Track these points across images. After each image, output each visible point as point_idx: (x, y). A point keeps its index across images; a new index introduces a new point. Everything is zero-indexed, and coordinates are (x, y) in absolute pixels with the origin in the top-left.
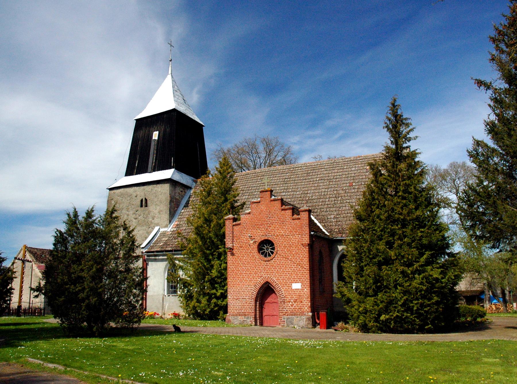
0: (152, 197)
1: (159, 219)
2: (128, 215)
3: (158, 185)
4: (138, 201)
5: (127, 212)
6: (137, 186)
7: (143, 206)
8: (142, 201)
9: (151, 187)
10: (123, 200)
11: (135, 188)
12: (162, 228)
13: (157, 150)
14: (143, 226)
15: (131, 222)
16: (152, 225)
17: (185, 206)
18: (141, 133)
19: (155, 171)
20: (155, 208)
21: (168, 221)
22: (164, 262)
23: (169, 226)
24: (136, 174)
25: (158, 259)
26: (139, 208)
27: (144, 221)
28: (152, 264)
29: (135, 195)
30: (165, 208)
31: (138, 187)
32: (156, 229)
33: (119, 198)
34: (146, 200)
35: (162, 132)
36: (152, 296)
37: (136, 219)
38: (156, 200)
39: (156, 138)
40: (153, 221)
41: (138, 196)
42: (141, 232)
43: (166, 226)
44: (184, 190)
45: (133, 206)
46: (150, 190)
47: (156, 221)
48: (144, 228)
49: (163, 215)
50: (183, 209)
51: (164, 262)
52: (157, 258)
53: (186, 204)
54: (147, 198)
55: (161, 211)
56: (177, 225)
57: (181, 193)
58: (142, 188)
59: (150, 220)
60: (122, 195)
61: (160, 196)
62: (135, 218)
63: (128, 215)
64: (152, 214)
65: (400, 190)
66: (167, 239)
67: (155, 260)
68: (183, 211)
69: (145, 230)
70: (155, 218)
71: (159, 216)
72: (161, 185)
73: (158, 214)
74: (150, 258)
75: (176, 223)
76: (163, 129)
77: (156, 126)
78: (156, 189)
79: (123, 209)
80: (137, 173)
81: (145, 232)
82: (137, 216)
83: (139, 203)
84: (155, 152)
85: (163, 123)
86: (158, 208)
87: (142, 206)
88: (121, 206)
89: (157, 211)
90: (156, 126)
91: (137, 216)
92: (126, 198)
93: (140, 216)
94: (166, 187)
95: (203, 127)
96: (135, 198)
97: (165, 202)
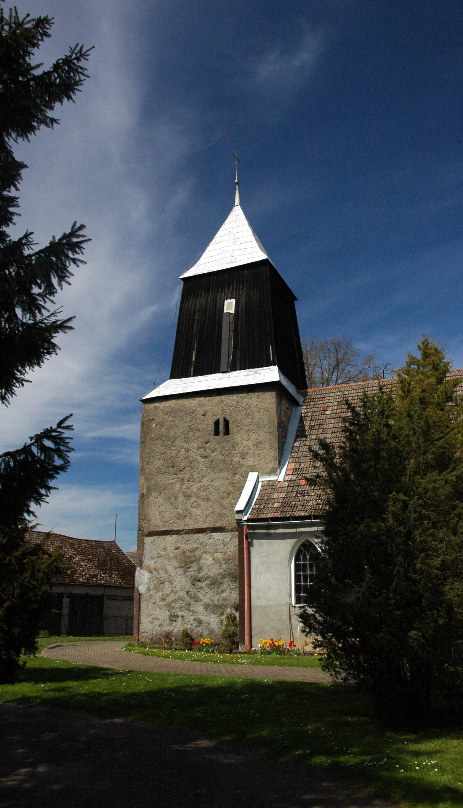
0: (239, 417)
1: (257, 458)
2: (188, 450)
3: (251, 395)
4: (209, 423)
5: (186, 445)
6: (205, 397)
7: (221, 433)
8: (217, 423)
9: (234, 398)
10: (176, 422)
11: (202, 398)
12: (263, 474)
13: (236, 331)
14: (221, 471)
15: (194, 463)
16: (242, 470)
17: (297, 436)
18: (199, 302)
19: (235, 370)
20: (245, 436)
21: (277, 462)
22: (289, 541)
23: (279, 471)
24: (194, 376)
25: (275, 533)
26: (212, 437)
27: (224, 461)
28: (260, 544)
29: (202, 412)
30: (268, 437)
31: (207, 398)
32: (252, 477)
33: (166, 417)
34: (226, 422)
35: (243, 301)
36: (264, 607)
37: (205, 457)
38: (248, 421)
39: (232, 311)
40: (243, 462)
41: (209, 415)
42: (217, 483)
43: (274, 472)
44: (290, 406)
45: (198, 434)
46: (234, 403)
47: (250, 461)
48: (225, 474)
49: (265, 451)
50: (295, 441)
51: (289, 541)
52: (273, 531)
53: (298, 431)
54: (228, 418)
55: (261, 442)
56: (295, 470)
57: (287, 410)
58: (217, 399)
59: (237, 459)
60: (173, 412)
61: (257, 416)
62: (204, 455)
63: (188, 450)
64: (239, 448)
65: (335, 453)
66: (283, 495)
67: (268, 537)
68: (297, 444)
69: (227, 478)
70: (247, 456)
71: (257, 452)
72: (257, 394)
73: (252, 448)
74: (256, 531)
75: (292, 466)
76: (244, 295)
77: (229, 289)
78: (246, 401)
79: (176, 438)
80: (196, 374)
81: (226, 482)
82: (208, 451)
83: (212, 428)
84: (232, 334)
85: (243, 286)
86: (253, 436)
87: (217, 433)
88: (172, 433)
89: (250, 443)
90: (229, 289)
91: (208, 451)
92: (181, 418)
93: (213, 452)
94: (270, 398)
95: (295, 302)
96: (203, 418)
97: (268, 426)
